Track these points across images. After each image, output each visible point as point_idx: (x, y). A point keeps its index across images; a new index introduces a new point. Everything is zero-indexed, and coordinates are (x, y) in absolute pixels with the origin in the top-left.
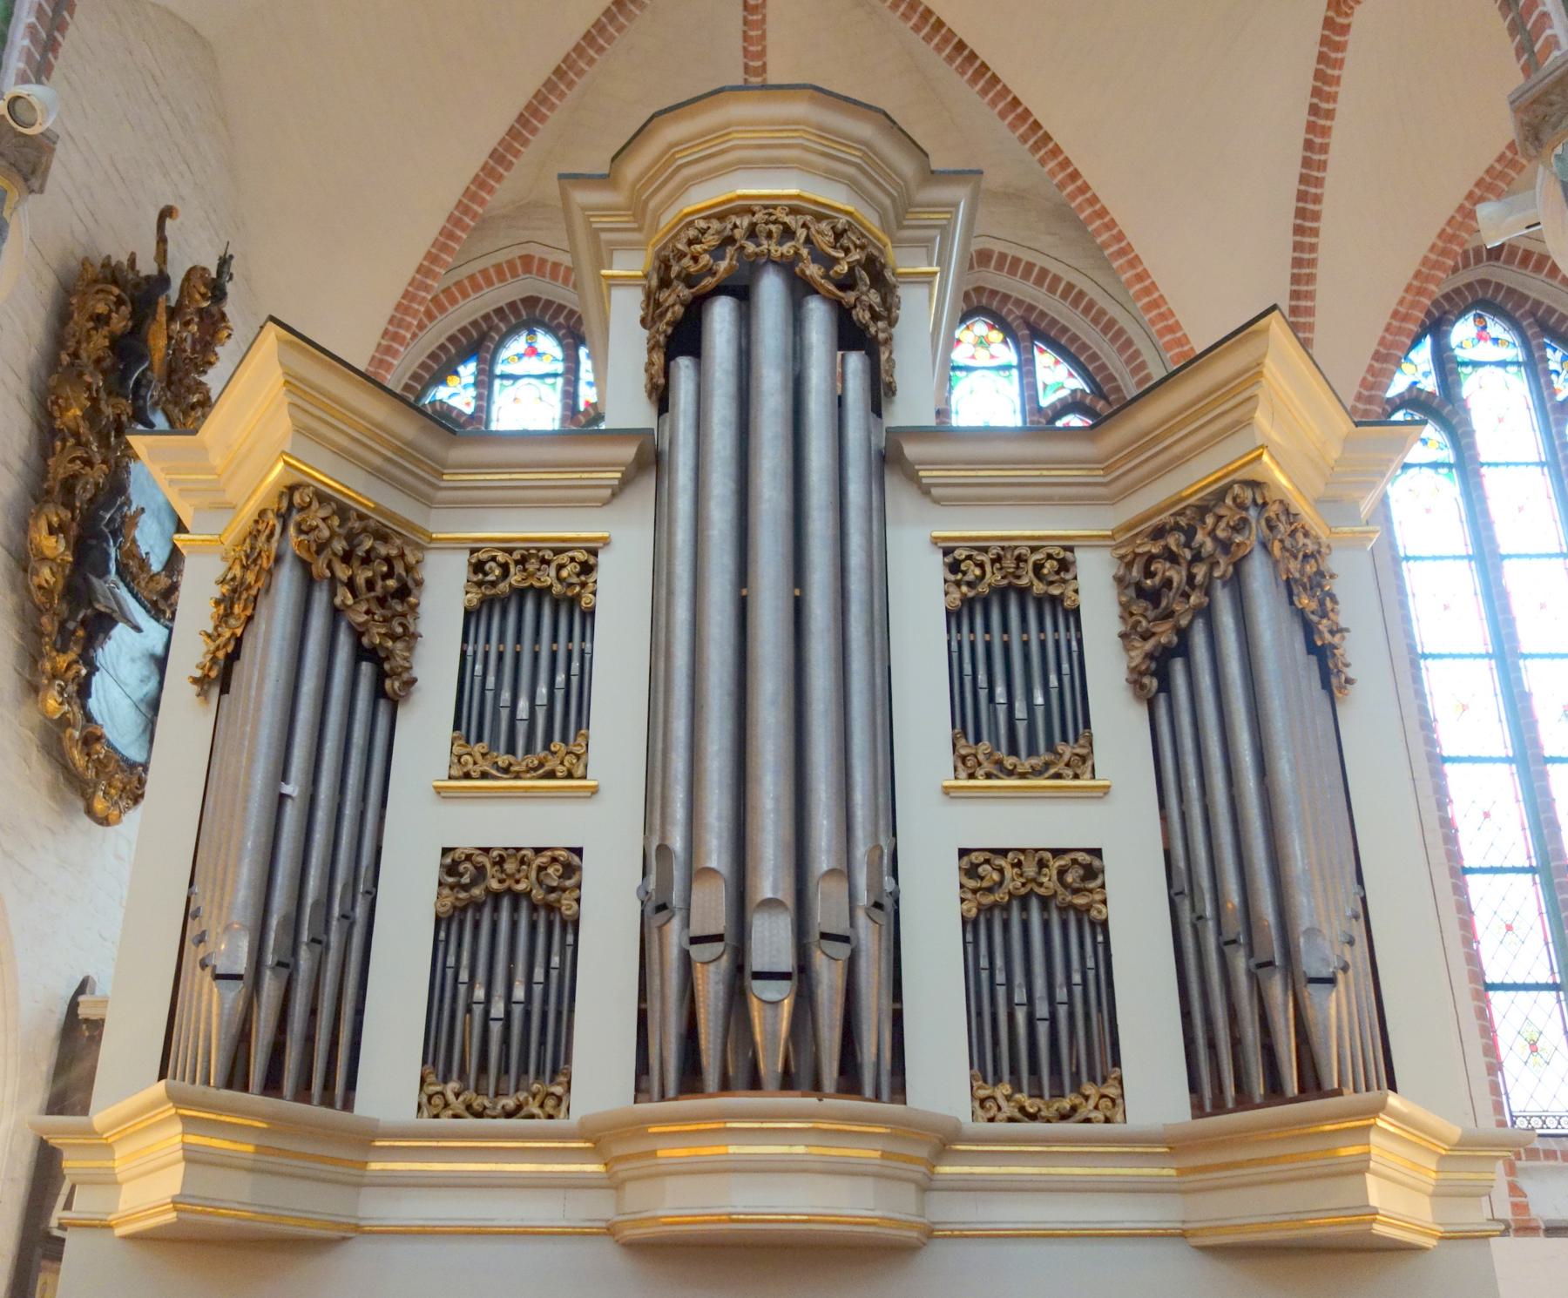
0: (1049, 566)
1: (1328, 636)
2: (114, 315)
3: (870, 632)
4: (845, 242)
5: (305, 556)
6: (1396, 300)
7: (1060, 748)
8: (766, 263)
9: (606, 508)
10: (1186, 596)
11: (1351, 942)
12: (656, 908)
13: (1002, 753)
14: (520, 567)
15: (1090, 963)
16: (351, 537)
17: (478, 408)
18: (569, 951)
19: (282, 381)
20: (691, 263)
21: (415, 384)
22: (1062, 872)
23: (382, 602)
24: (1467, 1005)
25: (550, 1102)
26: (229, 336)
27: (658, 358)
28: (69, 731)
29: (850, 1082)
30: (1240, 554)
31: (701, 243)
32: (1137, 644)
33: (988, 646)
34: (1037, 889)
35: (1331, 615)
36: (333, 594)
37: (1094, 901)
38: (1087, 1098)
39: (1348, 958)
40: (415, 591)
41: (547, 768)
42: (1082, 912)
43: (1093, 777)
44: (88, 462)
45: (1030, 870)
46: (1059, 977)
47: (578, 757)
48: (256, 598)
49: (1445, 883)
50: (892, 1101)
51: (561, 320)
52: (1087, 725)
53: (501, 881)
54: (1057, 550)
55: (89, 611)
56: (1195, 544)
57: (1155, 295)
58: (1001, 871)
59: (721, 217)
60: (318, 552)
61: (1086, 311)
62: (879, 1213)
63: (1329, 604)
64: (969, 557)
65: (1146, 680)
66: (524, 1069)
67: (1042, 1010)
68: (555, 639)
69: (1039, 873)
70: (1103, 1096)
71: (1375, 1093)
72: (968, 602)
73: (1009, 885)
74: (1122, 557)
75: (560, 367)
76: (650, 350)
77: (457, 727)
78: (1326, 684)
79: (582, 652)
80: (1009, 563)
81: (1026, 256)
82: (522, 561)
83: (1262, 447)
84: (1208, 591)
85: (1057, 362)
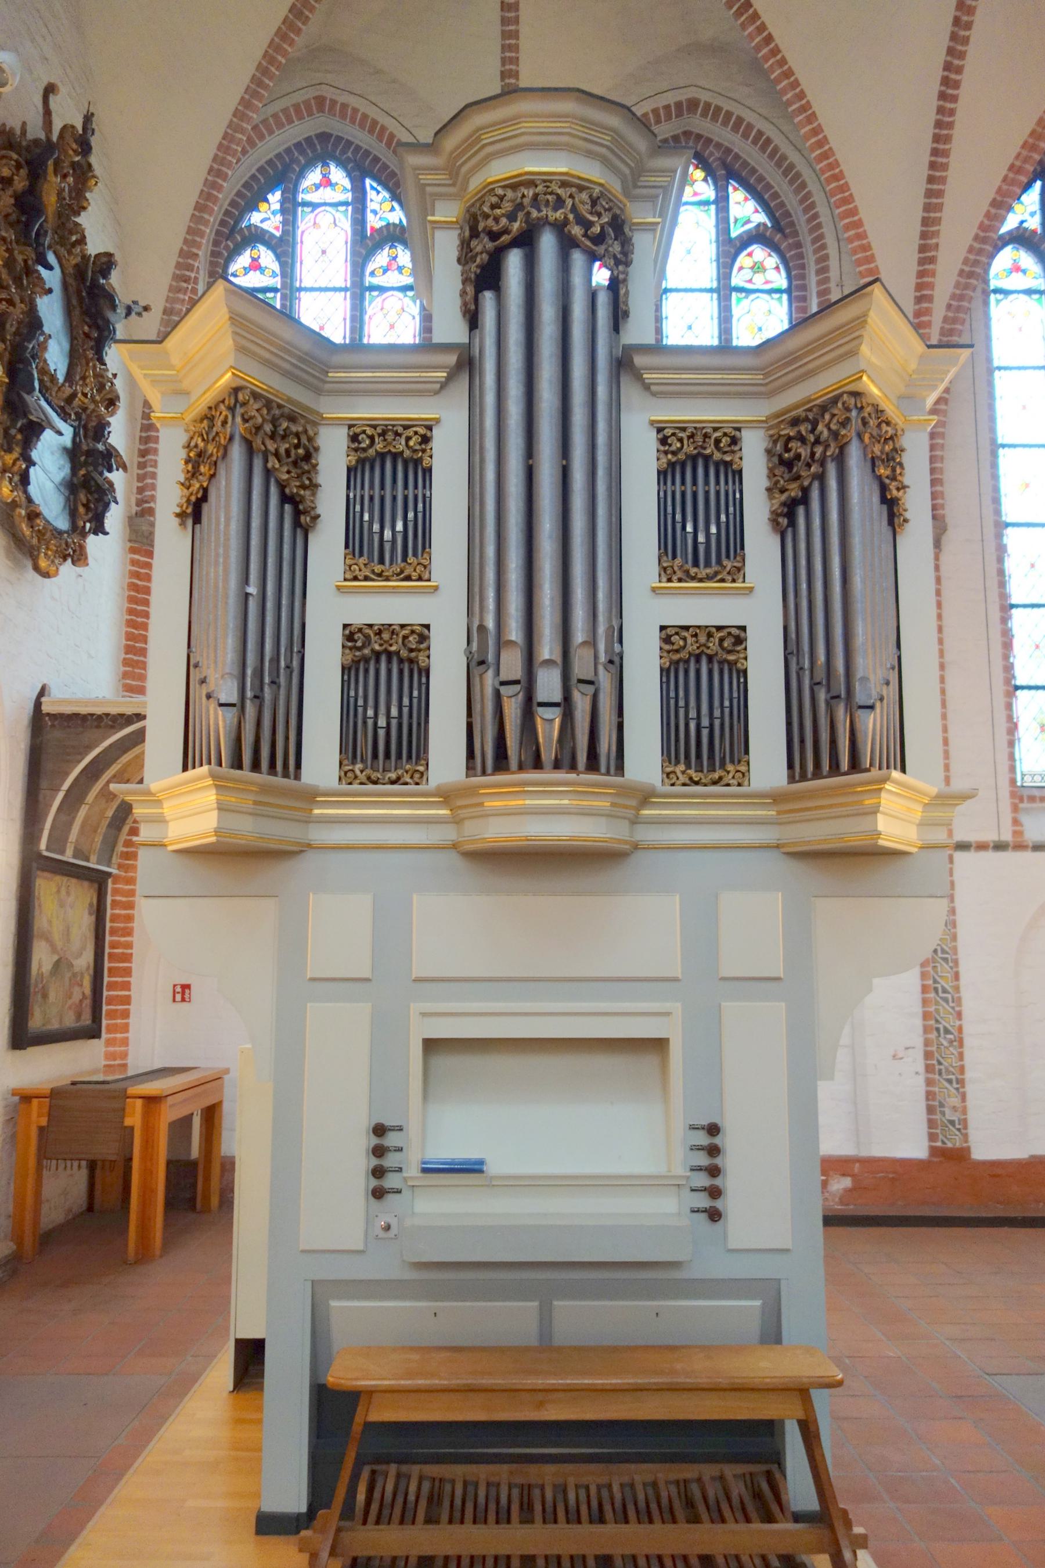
0: (725, 441)
1: (895, 492)
2: (16, 178)
3: (609, 489)
4: (598, 208)
5: (248, 436)
6: (1014, 155)
7: (725, 562)
8: (544, 225)
9: (436, 397)
10: (809, 466)
11: (888, 683)
12: (476, 664)
13: (689, 566)
14: (381, 438)
15: (735, 695)
16: (274, 422)
17: (285, 232)
18: (424, 687)
19: (227, 316)
20: (493, 223)
21: (233, 210)
22: (722, 640)
23: (295, 463)
24: (1000, 700)
25: (417, 776)
26: (96, 184)
27: (470, 290)
28: (18, 510)
29: (593, 764)
30: (844, 441)
31: (500, 208)
32: (777, 496)
33: (683, 494)
34: (706, 651)
35: (899, 478)
36: (266, 461)
37: (739, 658)
38: (728, 772)
39: (885, 693)
40: (314, 455)
41: (406, 573)
42: (732, 664)
43: (744, 582)
44: (10, 302)
45: (702, 639)
46: (717, 703)
47: (425, 567)
48: (215, 463)
49: (995, 615)
50: (616, 775)
51: (350, 154)
52: (742, 548)
53: (381, 645)
54: (730, 430)
55: (25, 421)
56: (817, 432)
57: (827, 147)
58: (685, 639)
59: (514, 187)
60: (256, 434)
61: (772, 156)
62: (608, 836)
63: (898, 471)
64: (673, 434)
65: (780, 520)
66: (399, 756)
67: (705, 722)
68: (406, 487)
69: (708, 640)
70: (738, 771)
71: (885, 771)
72: (672, 465)
73: (689, 648)
74: (771, 436)
75: (349, 196)
76: (464, 282)
77: (347, 546)
78: (891, 523)
79: (424, 496)
80: (699, 439)
81: (726, 105)
82: (383, 434)
83: (863, 371)
84: (822, 463)
85: (746, 199)
